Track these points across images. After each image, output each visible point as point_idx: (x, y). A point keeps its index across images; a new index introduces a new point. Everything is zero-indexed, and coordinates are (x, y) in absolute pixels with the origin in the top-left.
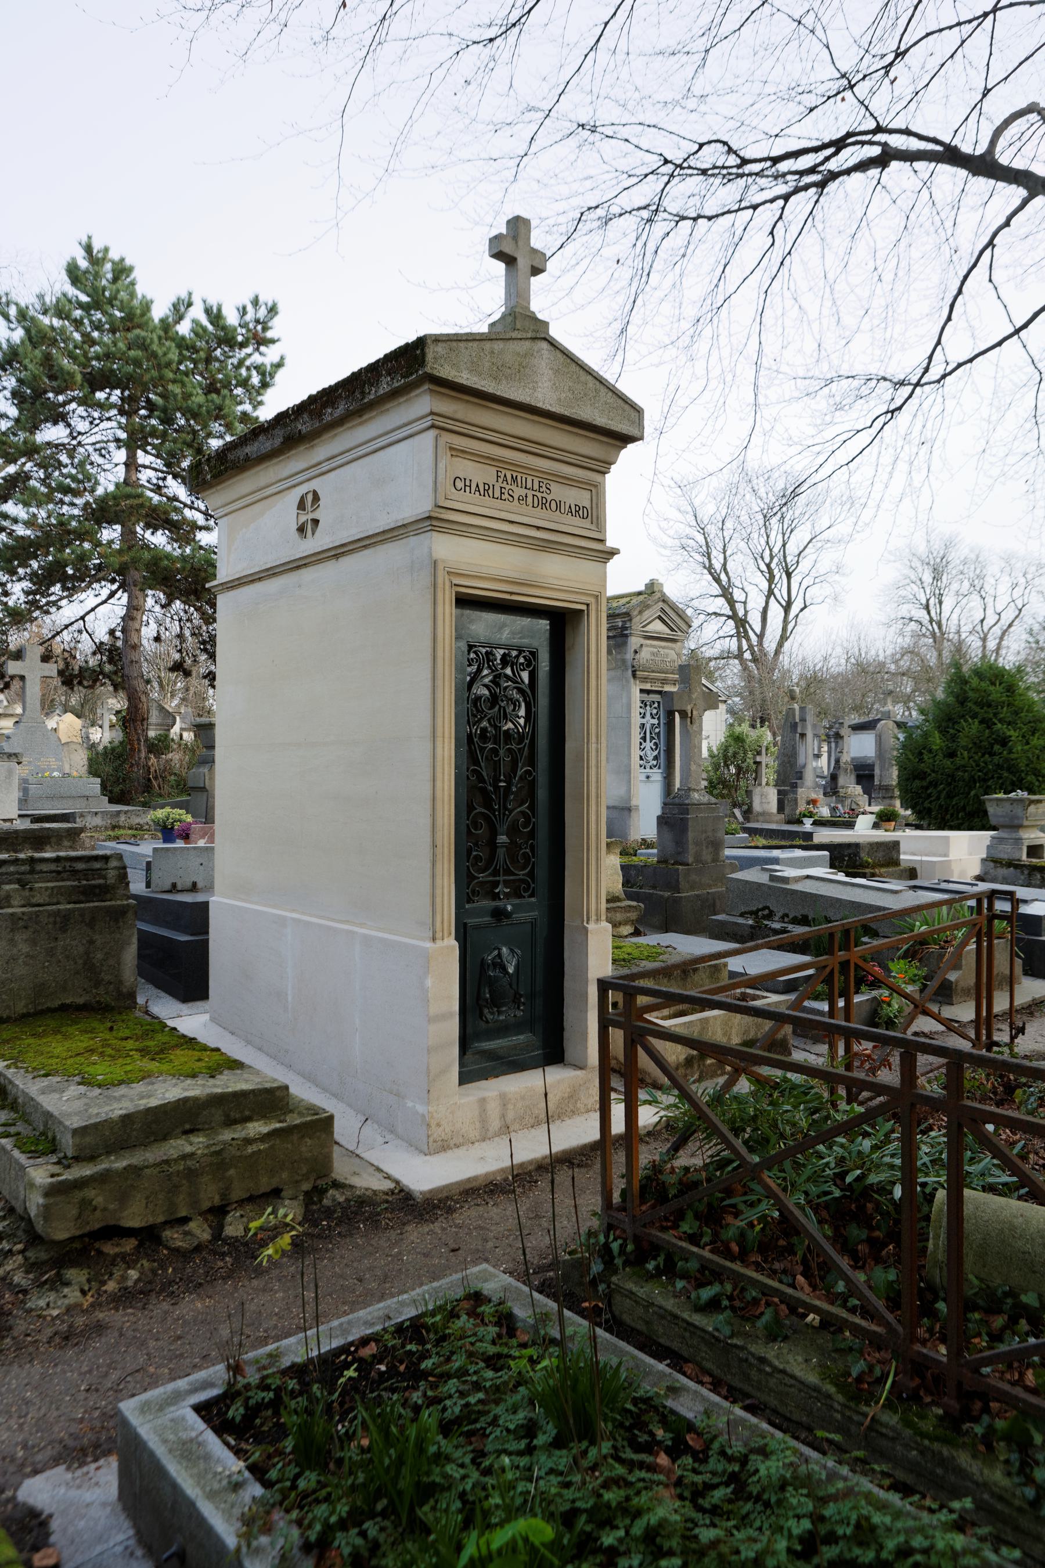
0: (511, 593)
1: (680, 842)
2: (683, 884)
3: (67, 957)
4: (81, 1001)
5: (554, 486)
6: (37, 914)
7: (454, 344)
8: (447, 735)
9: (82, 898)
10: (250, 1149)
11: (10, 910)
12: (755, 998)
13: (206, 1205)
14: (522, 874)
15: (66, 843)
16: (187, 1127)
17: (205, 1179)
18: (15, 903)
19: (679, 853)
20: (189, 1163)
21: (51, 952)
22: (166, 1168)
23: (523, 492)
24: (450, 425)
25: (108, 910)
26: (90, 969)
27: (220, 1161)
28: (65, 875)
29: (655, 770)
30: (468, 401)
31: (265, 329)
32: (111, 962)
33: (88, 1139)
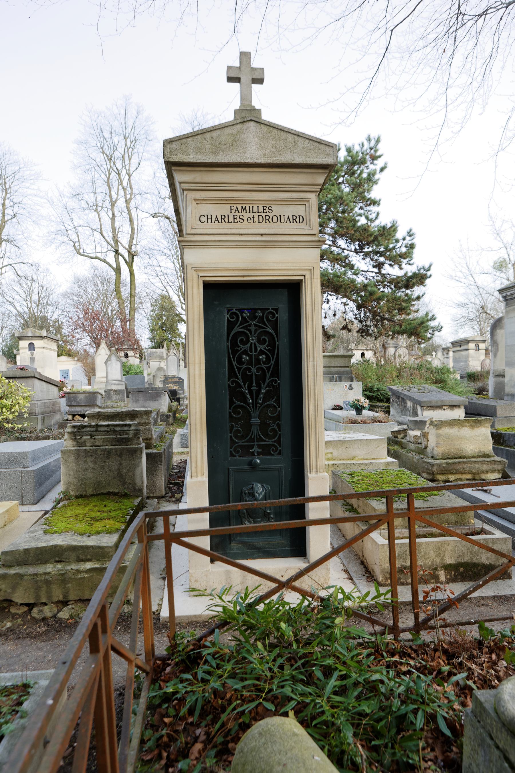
0: (243, 276)
3: (110, 470)
6: (96, 450)
7: (184, 140)
8: (197, 361)
9: (117, 443)
10: (80, 576)
11: (85, 448)
12: (483, 531)
13: (55, 599)
14: (271, 441)
15: (145, 417)
16: (57, 559)
18: (88, 444)
20: (47, 577)
21: (103, 468)
22: (35, 577)
23: (251, 215)
25: (128, 450)
26: (120, 476)
27: (63, 579)
28: (110, 433)
30: (200, 171)
31: (376, 151)
32: (130, 474)
33: (8, 557)
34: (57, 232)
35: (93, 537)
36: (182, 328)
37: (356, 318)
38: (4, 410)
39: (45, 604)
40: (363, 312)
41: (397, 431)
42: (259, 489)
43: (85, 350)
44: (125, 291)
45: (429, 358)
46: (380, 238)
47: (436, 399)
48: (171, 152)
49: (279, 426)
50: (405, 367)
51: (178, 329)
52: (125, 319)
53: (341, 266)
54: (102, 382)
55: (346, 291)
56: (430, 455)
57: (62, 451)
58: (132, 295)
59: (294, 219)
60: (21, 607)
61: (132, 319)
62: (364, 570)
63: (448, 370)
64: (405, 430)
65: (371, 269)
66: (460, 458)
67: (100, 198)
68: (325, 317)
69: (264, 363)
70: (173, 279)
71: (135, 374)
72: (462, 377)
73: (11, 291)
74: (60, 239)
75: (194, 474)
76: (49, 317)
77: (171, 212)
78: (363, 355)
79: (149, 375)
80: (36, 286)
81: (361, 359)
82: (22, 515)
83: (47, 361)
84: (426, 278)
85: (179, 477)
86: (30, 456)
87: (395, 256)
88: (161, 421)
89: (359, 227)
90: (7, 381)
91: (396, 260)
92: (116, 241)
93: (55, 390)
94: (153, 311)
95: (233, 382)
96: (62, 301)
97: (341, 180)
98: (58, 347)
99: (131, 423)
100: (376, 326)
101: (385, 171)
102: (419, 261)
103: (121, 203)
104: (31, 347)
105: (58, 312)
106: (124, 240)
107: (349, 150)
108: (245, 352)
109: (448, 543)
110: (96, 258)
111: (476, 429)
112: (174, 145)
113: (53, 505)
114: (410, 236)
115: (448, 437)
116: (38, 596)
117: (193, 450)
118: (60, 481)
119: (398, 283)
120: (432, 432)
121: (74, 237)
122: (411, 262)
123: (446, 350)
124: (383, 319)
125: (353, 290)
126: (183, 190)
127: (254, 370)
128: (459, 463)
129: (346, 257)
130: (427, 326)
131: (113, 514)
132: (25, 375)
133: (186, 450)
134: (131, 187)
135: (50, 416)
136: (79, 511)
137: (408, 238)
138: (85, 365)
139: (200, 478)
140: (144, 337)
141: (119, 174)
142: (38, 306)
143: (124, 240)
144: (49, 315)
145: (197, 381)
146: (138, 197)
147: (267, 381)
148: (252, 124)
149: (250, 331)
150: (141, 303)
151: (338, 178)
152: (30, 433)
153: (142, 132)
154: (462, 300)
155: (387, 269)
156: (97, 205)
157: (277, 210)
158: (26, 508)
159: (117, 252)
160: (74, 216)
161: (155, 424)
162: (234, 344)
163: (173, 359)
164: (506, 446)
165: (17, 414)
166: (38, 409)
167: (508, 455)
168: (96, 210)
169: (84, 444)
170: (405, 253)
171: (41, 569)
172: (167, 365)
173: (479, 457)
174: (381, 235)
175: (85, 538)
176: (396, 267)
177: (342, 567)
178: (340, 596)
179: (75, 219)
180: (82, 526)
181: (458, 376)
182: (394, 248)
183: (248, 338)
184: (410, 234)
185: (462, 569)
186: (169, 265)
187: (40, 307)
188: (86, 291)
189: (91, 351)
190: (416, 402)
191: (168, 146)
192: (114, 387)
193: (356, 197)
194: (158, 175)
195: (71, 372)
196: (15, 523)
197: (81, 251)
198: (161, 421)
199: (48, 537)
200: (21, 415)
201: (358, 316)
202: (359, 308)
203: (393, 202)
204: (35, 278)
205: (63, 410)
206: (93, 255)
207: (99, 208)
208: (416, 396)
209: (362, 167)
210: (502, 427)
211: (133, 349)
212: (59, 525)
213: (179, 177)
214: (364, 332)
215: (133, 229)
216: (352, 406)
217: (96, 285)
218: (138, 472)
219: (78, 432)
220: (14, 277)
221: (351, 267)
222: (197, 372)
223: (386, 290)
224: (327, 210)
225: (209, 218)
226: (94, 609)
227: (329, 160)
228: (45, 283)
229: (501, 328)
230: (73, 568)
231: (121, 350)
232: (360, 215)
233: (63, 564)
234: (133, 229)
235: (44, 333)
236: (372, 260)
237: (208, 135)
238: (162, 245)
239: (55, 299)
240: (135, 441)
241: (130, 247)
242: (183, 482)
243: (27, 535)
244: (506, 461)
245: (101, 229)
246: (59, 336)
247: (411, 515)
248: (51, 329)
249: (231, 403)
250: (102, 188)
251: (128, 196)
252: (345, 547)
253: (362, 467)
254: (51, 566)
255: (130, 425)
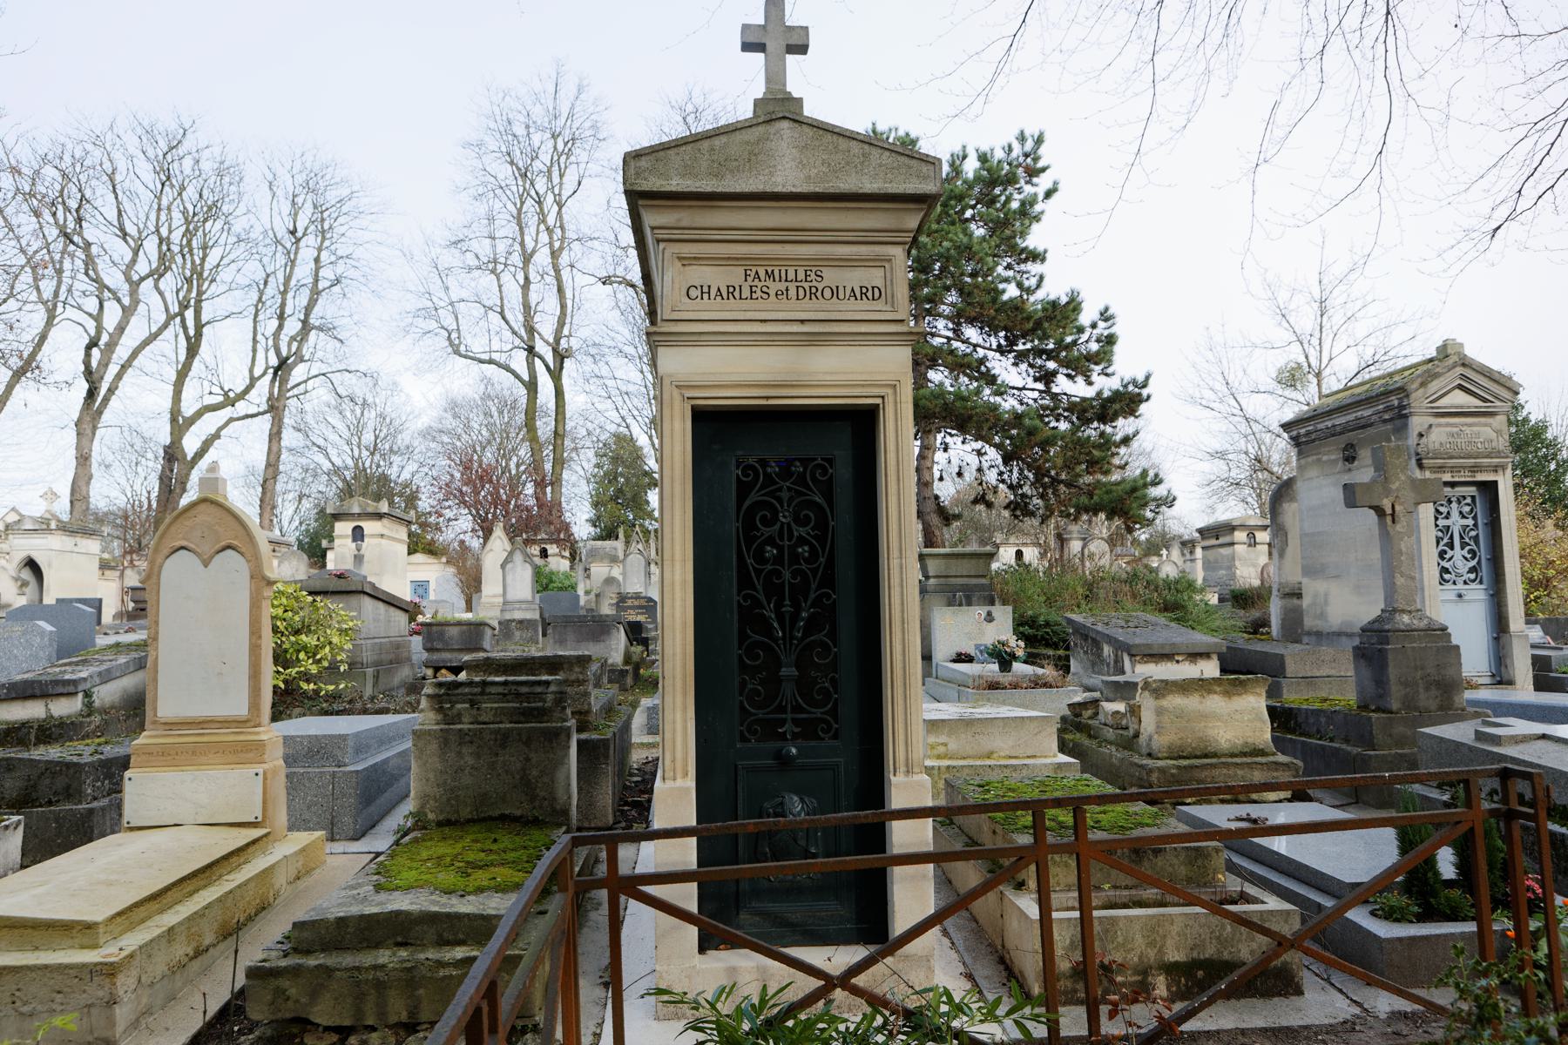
0: (768, 398)
1: (1380, 681)
2: (1379, 737)
4: (518, 813)
5: (826, 272)
7: (662, 153)
8: (678, 556)
12: (1244, 898)
13: (393, 1019)
14: (818, 713)
15: (577, 669)
16: (399, 939)
17: (392, 992)
18: (465, 720)
19: (1381, 696)
23: (783, 285)
24: (677, 234)
26: (526, 785)
29: (1473, 586)
31: (1036, 160)
32: (546, 780)
33: (306, 934)
34: (419, 313)
35: (471, 898)
36: (653, 497)
37: (1003, 481)
38: (302, 655)
39: (373, 1029)
40: (1016, 470)
41: (1079, 704)
42: (796, 805)
43: (462, 542)
44: (545, 427)
45: (1154, 562)
46: (1046, 325)
47: (1161, 641)
48: (637, 174)
49: (834, 682)
50: (1103, 579)
51: (648, 502)
52: (543, 480)
53: (971, 378)
54: (493, 605)
55: (979, 428)
56: (1144, 751)
57: (414, 732)
58: (559, 434)
59: (863, 293)
60: (326, 1035)
61: (556, 482)
62: (1004, 974)
63: (1190, 585)
64: (1096, 702)
65: (1031, 384)
66: (1206, 756)
67: (501, 247)
68: (941, 479)
69: (807, 561)
70: (640, 402)
71: (560, 589)
72: (1220, 600)
73: (323, 426)
74: (423, 325)
75: (669, 774)
76: (393, 477)
77: (636, 275)
78: (1019, 554)
79: (587, 593)
80: (371, 415)
81: (1013, 562)
82: (330, 859)
83: (389, 561)
84: (1141, 401)
85: (643, 792)
86: (351, 743)
87: (1078, 359)
88: (610, 681)
89: (1005, 303)
90: (310, 599)
91: (1080, 366)
92: (531, 330)
93: (401, 618)
94: (598, 466)
95: (745, 598)
96: (420, 445)
97: (969, 213)
98: (410, 535)
99: (550, 678)
100: (1042, 496)
101: (1056, 197)
102: (1125, 367)
103: (542, 258)
104: (358, 534)
105: (412, 467)
106: (546, 327)
107: (983, 158)
108: (770, 541)
109: (1171, 919)
110: (491, 362)
111: (1235, 698)
112: (643, 163)
113: (392, 839)
114: (1106, 320)
115: (1180, 714)
116: (359, 1013)
117: (668, 736)
118: (407, 796)
119: (1085, 411)
120: (1146, 702)
121: (449, 322)
122: (1109, 371)
123: (1187, 545)
124: (1055, 481)
125: (995, 425)
126: (658, 241)
127: (787, 575)
128: (1204, 767)
129: (982, 361)
130: (1145, 496)
131: (511, 856)
132: (347, 588)
133: (658, 739)
134: (562, 227)
135: (389, 670)
136: (444, 849)
137: (1102, 324)
138: (461, 571)
139: (679, 782)
140: (580, 517)
141: (540, 203)
142: (372, 454)
143: (546, 327)
144: (393, 472)
145: (678, 595)
146: (576, 246)
147: (812, 596)
148: (785, 124)
149: (780, 500)
150: (576, 449)
151: (963, 211)
152: (350, 702)
153: (587, 124)
154: (1216, 445)
155: (1062, 384)
156: (495, 261)
157: (831, 277)
158: (338, 847)
159: (531, 350)
160: (451, 282)
161: (597, 685)
162: (749, 525)
163: (636, 560)
164: (1301, 735)
165: (326, 664)
166: (367, 656)
167: (1306, 753)
168: (493, 271)
169: (458, 718)
170: (1098, 353)
171: (367, 959)
172: (624, 574)
173: (1244, 754)
174: (1050, 319)
175: (454, 900)
176: (1080, 379)
177: (962, 969)
178: (944, 1008)
179: (452, 288)
180: (448, 878)
181: (1214, 599)
182: (1075, 343)
183: (775, 513)
184: (1106, 316)
185: (1200, 973)
186: (632, 374)
187: (377, 457)
188: (467, 427)
189: (475, 543)
190: (1121, 647)
191: (632, 164)
192: (518, 615)
193: (998, 246)
194: (614, 203)
195: (432, 586)
196: (317, 874)
197: (462, 348)
198: (610, 681)
199: (383, 896)
200: (333, 666)
201: (1005, 476)
202: (1007, 459)
203: (1071, 254)
204: (370, 400)
205: (414, 658)
206: (485, 357)
207: (500, 267)
208: (1121, 635)
209: (1010, 189)
210: (1293, 697)
211: (557, 541)
212: (405, 875)
213: (650, 219)
214: (1019, 508)
215: (563, 306)
216: (990, 655)
217: (488, 414)
218: (560, 776)
219: (446, 697)
220: (330, 398)
221: (991, 379)
222: (678, 577)
223: (1063, 426)
224: (942, 270)
225: (705, 291)
226: (477, 982)
227: (930, 187)
228: (388, 410)
229: (1293, 499)
230: (430, 956)
231: (534, 542)
232: (1007, 280)
233: (411, 949)
234: (563, 306)
235: (384, 507)
236: (1031, 366)
237: (706, 144)
238: (619, 337)
239: (407, 442)
240: (556, 715)
241: (557, 340)
242: (650, 801)
243: (343, 893)
244: (1300, 763)
245: (502, 307)
246: (412, 513)
247: (1080, 850)
248: (397, 499)
249: (743, 636)
250: (508, 229)
251: (557, 245)
252: (954, 907)
253: (1007, 772)
254: (388, 953)
255: (547, 683)
